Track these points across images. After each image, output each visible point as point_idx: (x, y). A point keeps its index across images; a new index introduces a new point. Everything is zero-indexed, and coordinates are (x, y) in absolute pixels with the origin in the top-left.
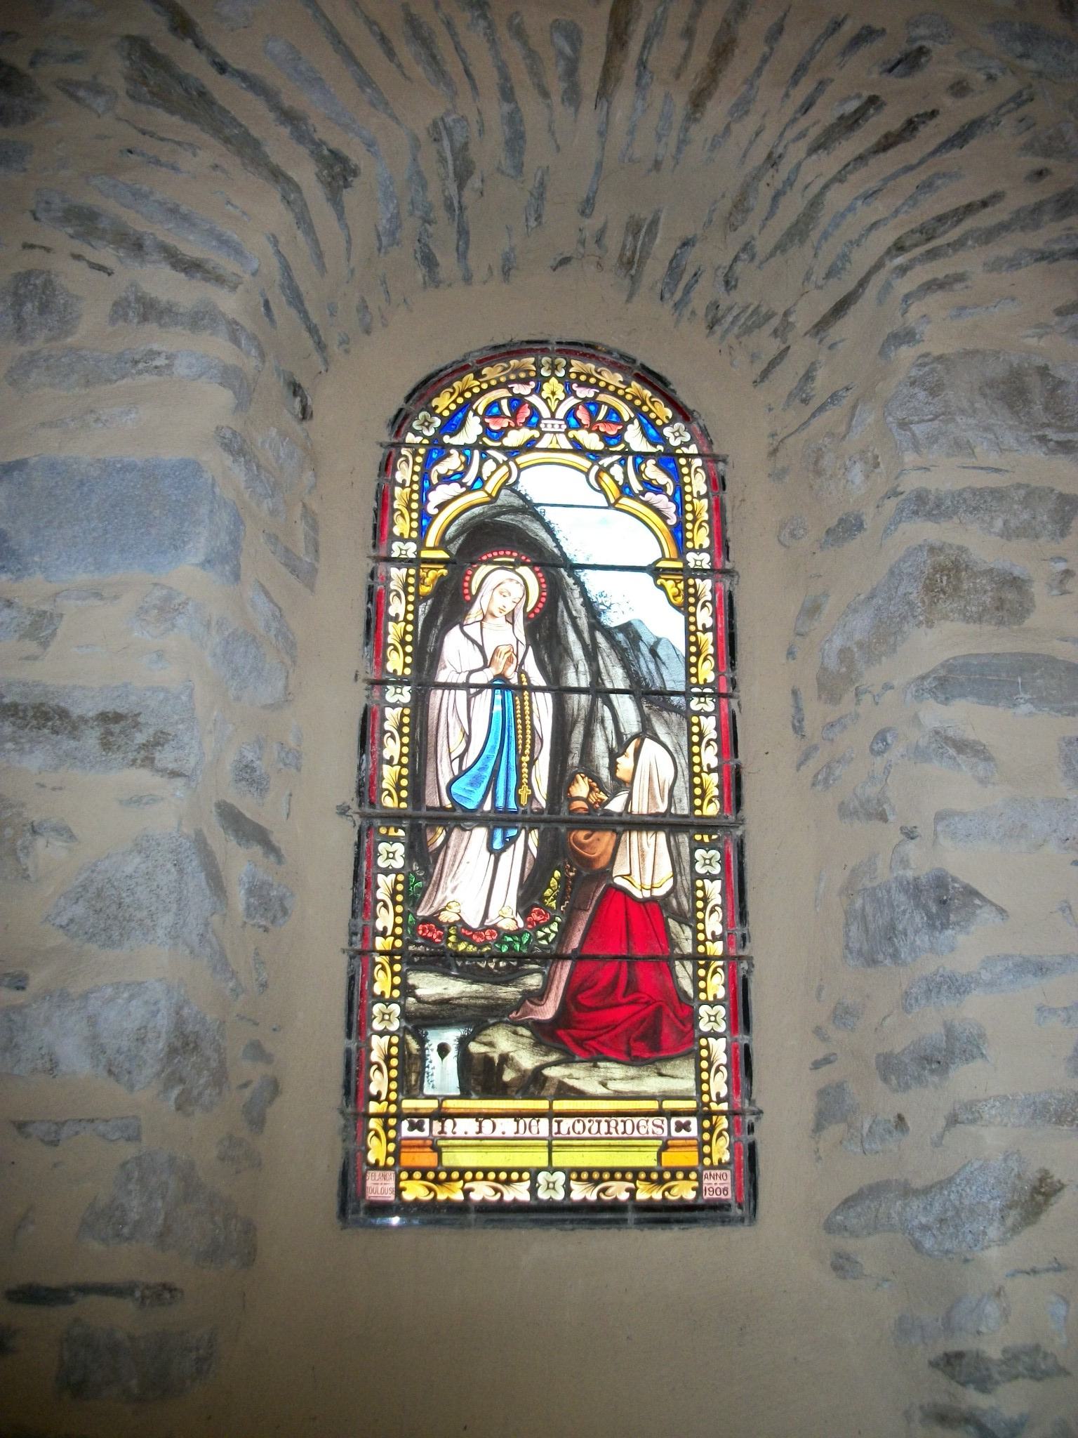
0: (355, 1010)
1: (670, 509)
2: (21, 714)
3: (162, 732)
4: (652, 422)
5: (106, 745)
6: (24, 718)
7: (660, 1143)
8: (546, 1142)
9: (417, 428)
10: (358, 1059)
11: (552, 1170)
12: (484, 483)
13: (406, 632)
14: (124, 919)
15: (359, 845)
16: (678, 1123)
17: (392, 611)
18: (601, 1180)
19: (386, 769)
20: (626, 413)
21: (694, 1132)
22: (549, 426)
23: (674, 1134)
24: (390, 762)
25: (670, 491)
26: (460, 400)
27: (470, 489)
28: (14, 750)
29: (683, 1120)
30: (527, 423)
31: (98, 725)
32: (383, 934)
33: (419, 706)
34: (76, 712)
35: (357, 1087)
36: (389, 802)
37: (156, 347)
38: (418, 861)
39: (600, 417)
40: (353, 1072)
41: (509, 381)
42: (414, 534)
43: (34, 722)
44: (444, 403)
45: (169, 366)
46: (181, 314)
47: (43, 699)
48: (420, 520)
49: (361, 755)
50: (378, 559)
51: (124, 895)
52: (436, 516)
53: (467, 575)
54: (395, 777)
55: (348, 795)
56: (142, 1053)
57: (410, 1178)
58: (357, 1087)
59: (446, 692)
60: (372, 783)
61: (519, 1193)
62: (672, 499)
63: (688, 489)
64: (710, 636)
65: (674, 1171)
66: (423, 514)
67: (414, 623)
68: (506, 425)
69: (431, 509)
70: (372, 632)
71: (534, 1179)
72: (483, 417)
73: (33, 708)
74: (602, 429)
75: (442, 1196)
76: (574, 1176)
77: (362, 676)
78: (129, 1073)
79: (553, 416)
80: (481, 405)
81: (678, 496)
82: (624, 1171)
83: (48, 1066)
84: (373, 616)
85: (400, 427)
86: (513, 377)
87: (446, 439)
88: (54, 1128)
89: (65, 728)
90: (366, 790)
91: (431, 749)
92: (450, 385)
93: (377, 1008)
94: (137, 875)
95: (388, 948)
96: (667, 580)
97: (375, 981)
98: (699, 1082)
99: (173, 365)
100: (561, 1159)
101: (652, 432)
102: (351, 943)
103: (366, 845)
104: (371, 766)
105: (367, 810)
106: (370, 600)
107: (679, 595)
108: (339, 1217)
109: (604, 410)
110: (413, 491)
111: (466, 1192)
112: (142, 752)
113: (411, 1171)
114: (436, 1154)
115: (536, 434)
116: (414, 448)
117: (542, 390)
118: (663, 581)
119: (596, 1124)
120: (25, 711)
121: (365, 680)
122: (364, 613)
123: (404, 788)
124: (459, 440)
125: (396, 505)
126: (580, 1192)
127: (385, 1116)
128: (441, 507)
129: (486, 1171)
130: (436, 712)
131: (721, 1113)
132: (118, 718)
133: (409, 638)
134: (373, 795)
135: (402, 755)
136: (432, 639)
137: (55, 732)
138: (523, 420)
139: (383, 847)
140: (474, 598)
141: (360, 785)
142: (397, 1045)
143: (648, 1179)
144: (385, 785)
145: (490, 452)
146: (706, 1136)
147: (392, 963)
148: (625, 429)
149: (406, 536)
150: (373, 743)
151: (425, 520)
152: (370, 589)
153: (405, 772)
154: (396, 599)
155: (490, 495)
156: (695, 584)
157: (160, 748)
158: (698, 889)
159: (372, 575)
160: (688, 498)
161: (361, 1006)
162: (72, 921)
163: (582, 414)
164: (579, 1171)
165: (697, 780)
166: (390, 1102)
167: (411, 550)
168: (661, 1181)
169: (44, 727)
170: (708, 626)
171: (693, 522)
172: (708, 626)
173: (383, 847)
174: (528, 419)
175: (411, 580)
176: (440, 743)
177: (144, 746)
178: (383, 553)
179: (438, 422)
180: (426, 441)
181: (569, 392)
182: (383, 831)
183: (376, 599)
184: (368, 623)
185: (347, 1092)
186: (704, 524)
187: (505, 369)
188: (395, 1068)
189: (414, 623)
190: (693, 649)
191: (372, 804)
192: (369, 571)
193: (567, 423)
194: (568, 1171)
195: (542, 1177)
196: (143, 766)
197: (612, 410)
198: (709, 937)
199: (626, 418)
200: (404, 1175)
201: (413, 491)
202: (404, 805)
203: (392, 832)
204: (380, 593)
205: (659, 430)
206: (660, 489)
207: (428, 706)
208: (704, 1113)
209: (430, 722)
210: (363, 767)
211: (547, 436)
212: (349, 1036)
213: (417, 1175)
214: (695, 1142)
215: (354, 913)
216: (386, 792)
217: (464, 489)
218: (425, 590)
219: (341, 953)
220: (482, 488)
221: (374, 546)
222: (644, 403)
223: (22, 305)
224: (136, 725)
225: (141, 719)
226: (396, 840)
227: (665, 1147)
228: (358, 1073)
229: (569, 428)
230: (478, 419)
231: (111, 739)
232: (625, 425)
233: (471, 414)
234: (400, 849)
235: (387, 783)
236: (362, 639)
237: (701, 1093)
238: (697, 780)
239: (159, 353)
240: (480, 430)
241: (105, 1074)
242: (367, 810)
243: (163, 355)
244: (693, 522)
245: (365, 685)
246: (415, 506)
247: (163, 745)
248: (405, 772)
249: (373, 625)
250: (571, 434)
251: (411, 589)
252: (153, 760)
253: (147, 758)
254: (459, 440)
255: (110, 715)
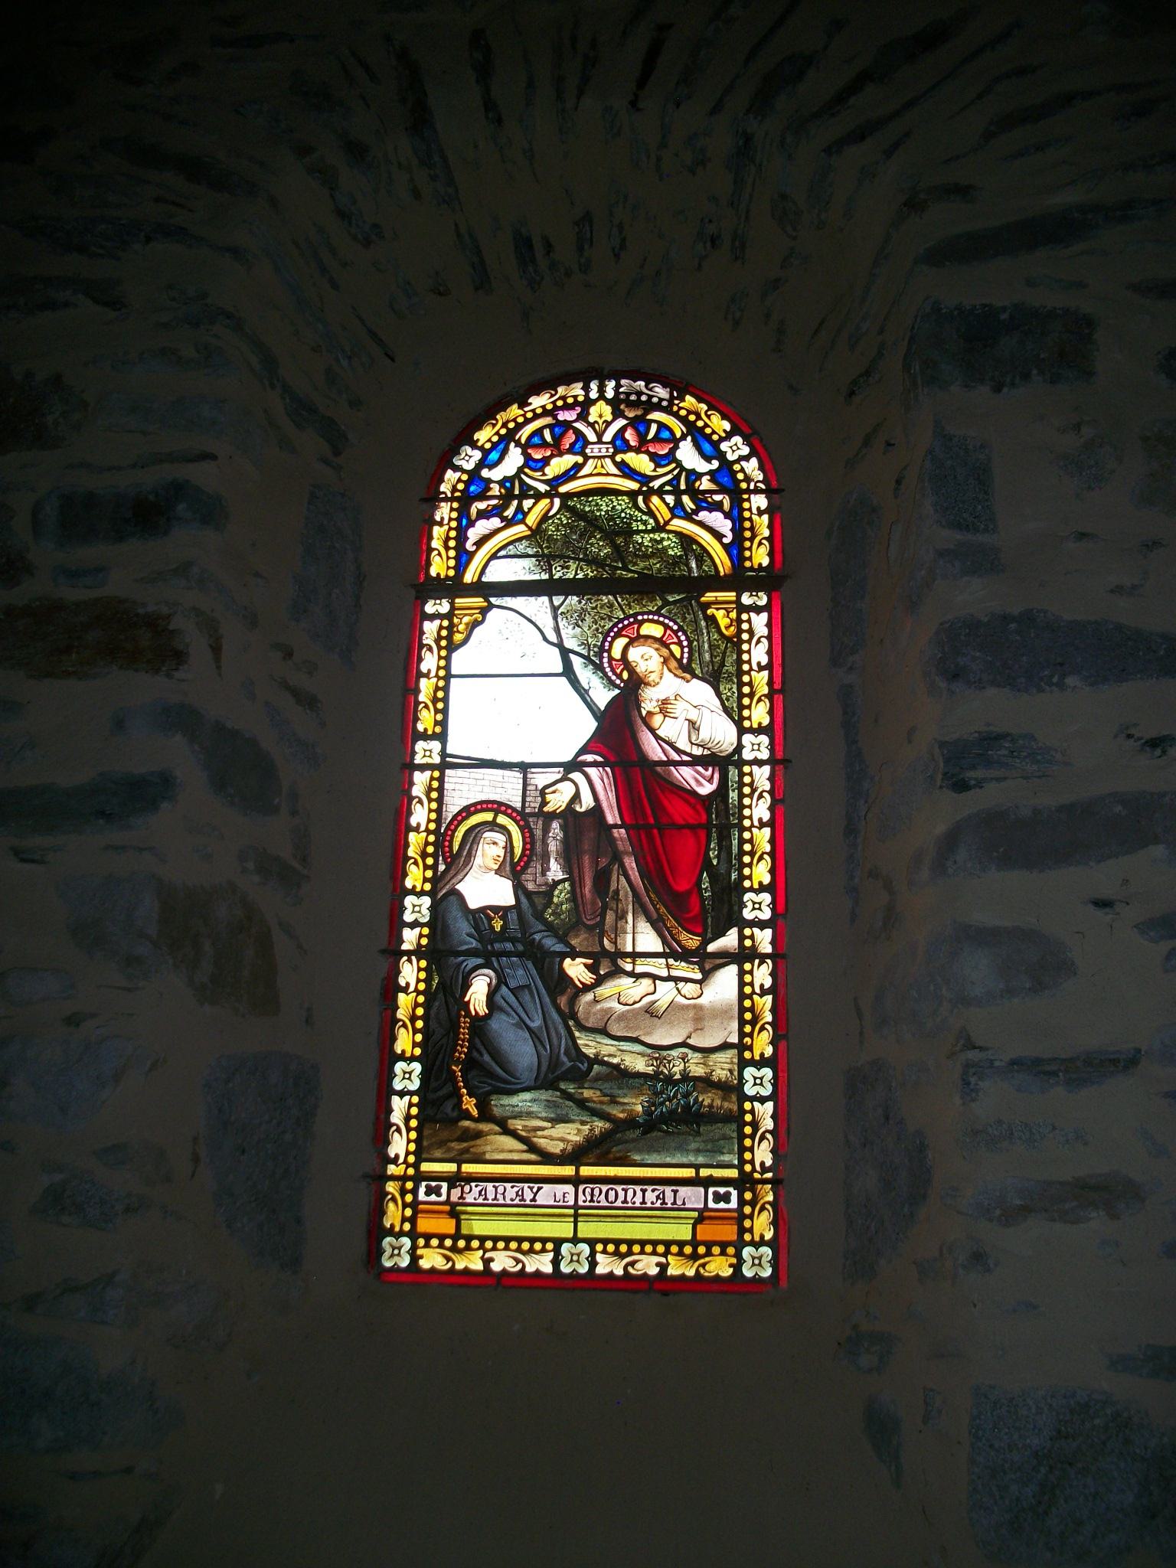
1: (725, 526)
4: (708, 438)
7: (695, 1214)
8: (571, 1211)
11: (575, 1240)
12: (526, 515)
16: (716, 1194)
18: (630, 1253)
20: (678, 429)
21: (734, 1204)
22: (596, 450)
23: (711, 1205)
25: (727, 505)
26: (503, 431)
29: (722, 1190)
30: (571, 450)
39: (651, 436)
48: (457, 558)
54: (422, 842)
57: (427, 1245)
61: (542, 1264)
62: (727, 516)
63: (747, 812)
64: (769, 998)
65: (709, 1245)
66: (460, 548)
71: (557, 1251)
74: (651, 450)
75: (460, 1265)
76: (599, 1247)
79: (600, 441)
80: (524, 434)
81: (735, 512)
82: (655, 1243)
96: (718, 609)
98: (742, 1035)
100: (587, 1230)
101: (707, 447)
107: (731, 625)
109: (654, 428)
111: (487, 1262)
113: (428, 1237)
114: (454, 1221)
115: (580, 459)
117: (588, 414)
118: (715, 611)
119: (629, 1199)
123: (419, 1018)
126: (606, 1265)
127: (404, 1178)
128: (480, 543)
129: (507, 1240)
131: (765, 1182)
138: (568, 446)
142: (413, 1153)
143: (680, 1253)
146: (747, 1210)
148: (676, 447)
155: (530, 528)
156: (750, 619)
158: (746, 1112)
160: (747, 514)
163: (629, 435)
164: (605, 1242)
165: (747, 1003)
166: (408, 1166)
168: (694, 1257)
170: (765, 820)
171: (752, 854)
172: (765, 820)
174: (573, 445)
181: (617, 414)
186: (764, 541)
188: (414, 1129)
190: (748, 1016)
193: (614, 447)
194: (592, 1242)
195: (566, 1248)
197: (662, 426)
198: (756, 823)
199: (678, 435)
200: (421, 1242)
201: (450, 529)
205: (715, 445)
206: (717, 507)
208: (745, 1182)
211: (591, 461)
213: (435, 1242)
214: (735, 1215)
216: (412, 861)
220: (523, 521)
222: (699, 417)
227: (700, 1220)
229: (617, 452)
232: (675, 442)
233: (512, 444)
237: (742, 1162)
238: (747, 1003)
240: (520, 460)
244: (752, 540)
248: (421, 999)
250: (618, 458)
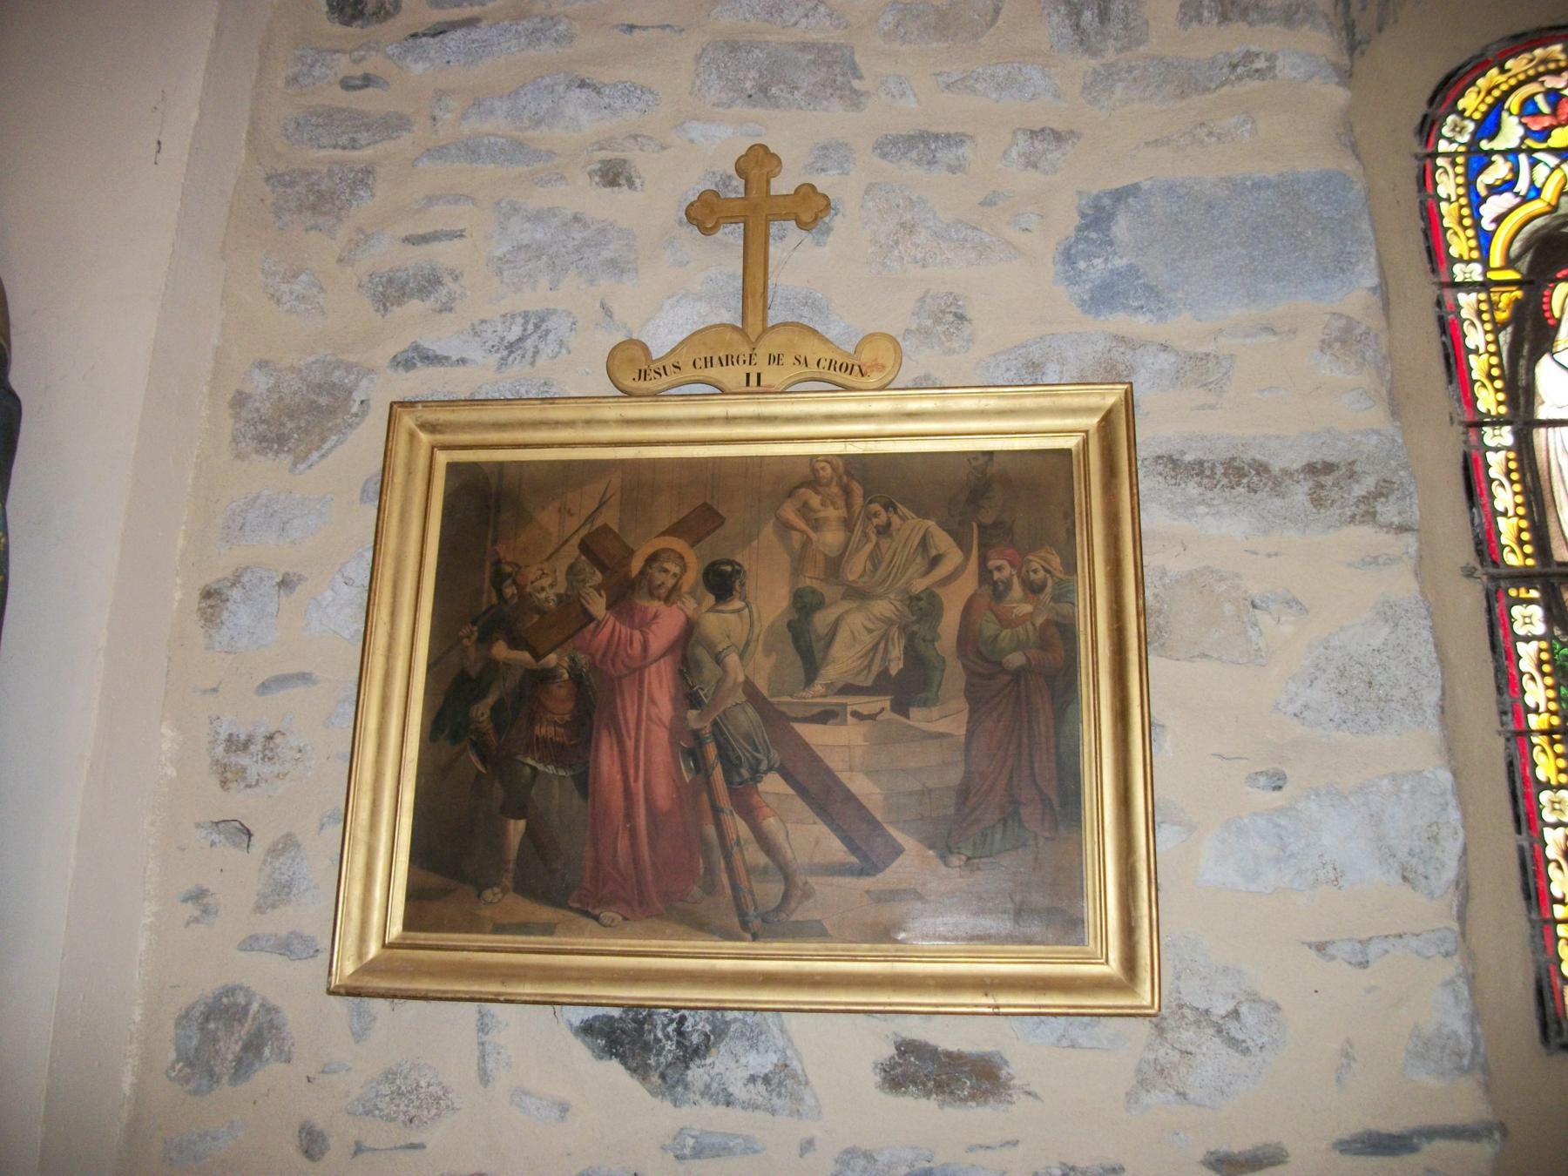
0: (1521, 800)
2: (1208, 472)
3: (1385, 481)
5: (1317, 501)
6: (1211, 477)
9: (1449, 135)
10: (1533, 857)
12: (1539, 191)
13: (1491, 366)
14: (1380, 700)
15: (1490, 610)
17: (1470, 343)
19: (1502, 523)
24: (1505, 514)
27: (1525, 200)
28: (1208, 514)
31: (1305, 479)
32: (1536, 711)
33: (1524, 448)
34: (1276, 466)
35: (1537, 889)
36: (1513, 559)
37: (1254, 48)
38: (1558, 625)
40: (1531, 874)
41: (1539, 75)
42: (1475, 254)
43: (1225, 481)
44: (1472, 102)
45: (1271, 68)
46: (1271, 9)
47: (1233, 453)
49: (1471, 509)
50: (1443, 285)
51: (1375, 672)
52: (1494, 232)
53: (1544, 296)
54: (1514, 531)
55: (1468, 556)
56: (1438, 853)
58: (1537, 889)
59: (1550, 430)
60: (1490, 540)
67: (1498, 353)
68: (1546, 124)
69: (1487, 225)
70: (1454, 368)
72: (1520, 115)
73: (1222, 464)
77: (1456, 419)
78: (1426, 878)
80: (1514, 102)
83: (1332, 876)
84: (1450, 350)
85: (1429, 135)
86: (1541, 69)
87: (1485, 145)
88: (1358, 946)
89: (1265, 485)
90: (1484, 547)
91: (1547, 497)
92: (1473, 83)
93: (1545, 797)
94: (1386, 648)
95: (1545, 726)
97: (1536, 765)
99: (1274, 67)
102: (1502, 724)
103: (1497, 610)
104: (1484, 520)
105: (1492, 570)
106: (1443, 331)
108: (1543, 1043)
110: (1461, 207)
112: (1362, 506)
116: (1451, 156)
120: (1213, 468)
121: (1461, 423)
122: (1440, 346)
124: (1500, 143)
125: (1446, 223)
128: (1499, 220)
130: (1544, 454)
132: (1329, 468)
133: (1495, 372)
134: (1494, 553)
135: (1517, 505)
136: (1522, 371)
137: (1252, 490)
139: (1517, 611)
140: (1559, 321)
141: (1478, 543)
144: (1504, 540)
145: (1538, 156)
147: (1552, 743)
149: (1466, 257)
150: (1482, 495)
151: (1484, 240)
152: (1441, 320)
153: (1524, 524)
154: (1471, 328)
157: (1383, 500)
159: (1439, 303)
161: (1527, 796)
162: (1306, 707)
167: (1475, 272)
169: (1239, 485)
173: (1517, 611)
175: (1484, 307)
176: (1555, 489)
177: (1364, 499)
178: (1444, 278)
179: (1471, 126)
180: (1462, 149)
182: (1513, 592)
183: (1450, 329)
184: (1447, 357)
185: (1528, 897)
187: (1531, 61)
189: (1498, 353)
191: (1495, 564)
192: (1435, 300)
196: (1362, 522)
202: (1530, 562)
203: (1523, 594)
204: (1452, 324)
207: (1533, 447)
209: (1539, 466)
210: (1477, 521)
212: (1519, 831)
215: (1499, 690)
217: (1518, 200)
218: (1502, 316)
219: (1497, 736)
221: (1433, 271)
223: (1079, 14)
224: (1352, 475)
225: (1357, 468)
226: (1530, 602)
228: (1537, 873)
230: (1515, 120)
231: (1324, 493)
234: (1537, 612)
235: (1507, 538)
236: (1444, 377)
239: (1258, 55)
240: (1520, 131)
241: (1400, 881)
242: (1492, 570)
243: (1263, 58)
245: (1461, 429)
246: (1467, 222)
247: (1386, 496)
249: (1452, 360)
251: (1486, 317)
252: (1374, 514)
253: (1367, 512)
254: (1500, 143)
255: (1319, 466)
